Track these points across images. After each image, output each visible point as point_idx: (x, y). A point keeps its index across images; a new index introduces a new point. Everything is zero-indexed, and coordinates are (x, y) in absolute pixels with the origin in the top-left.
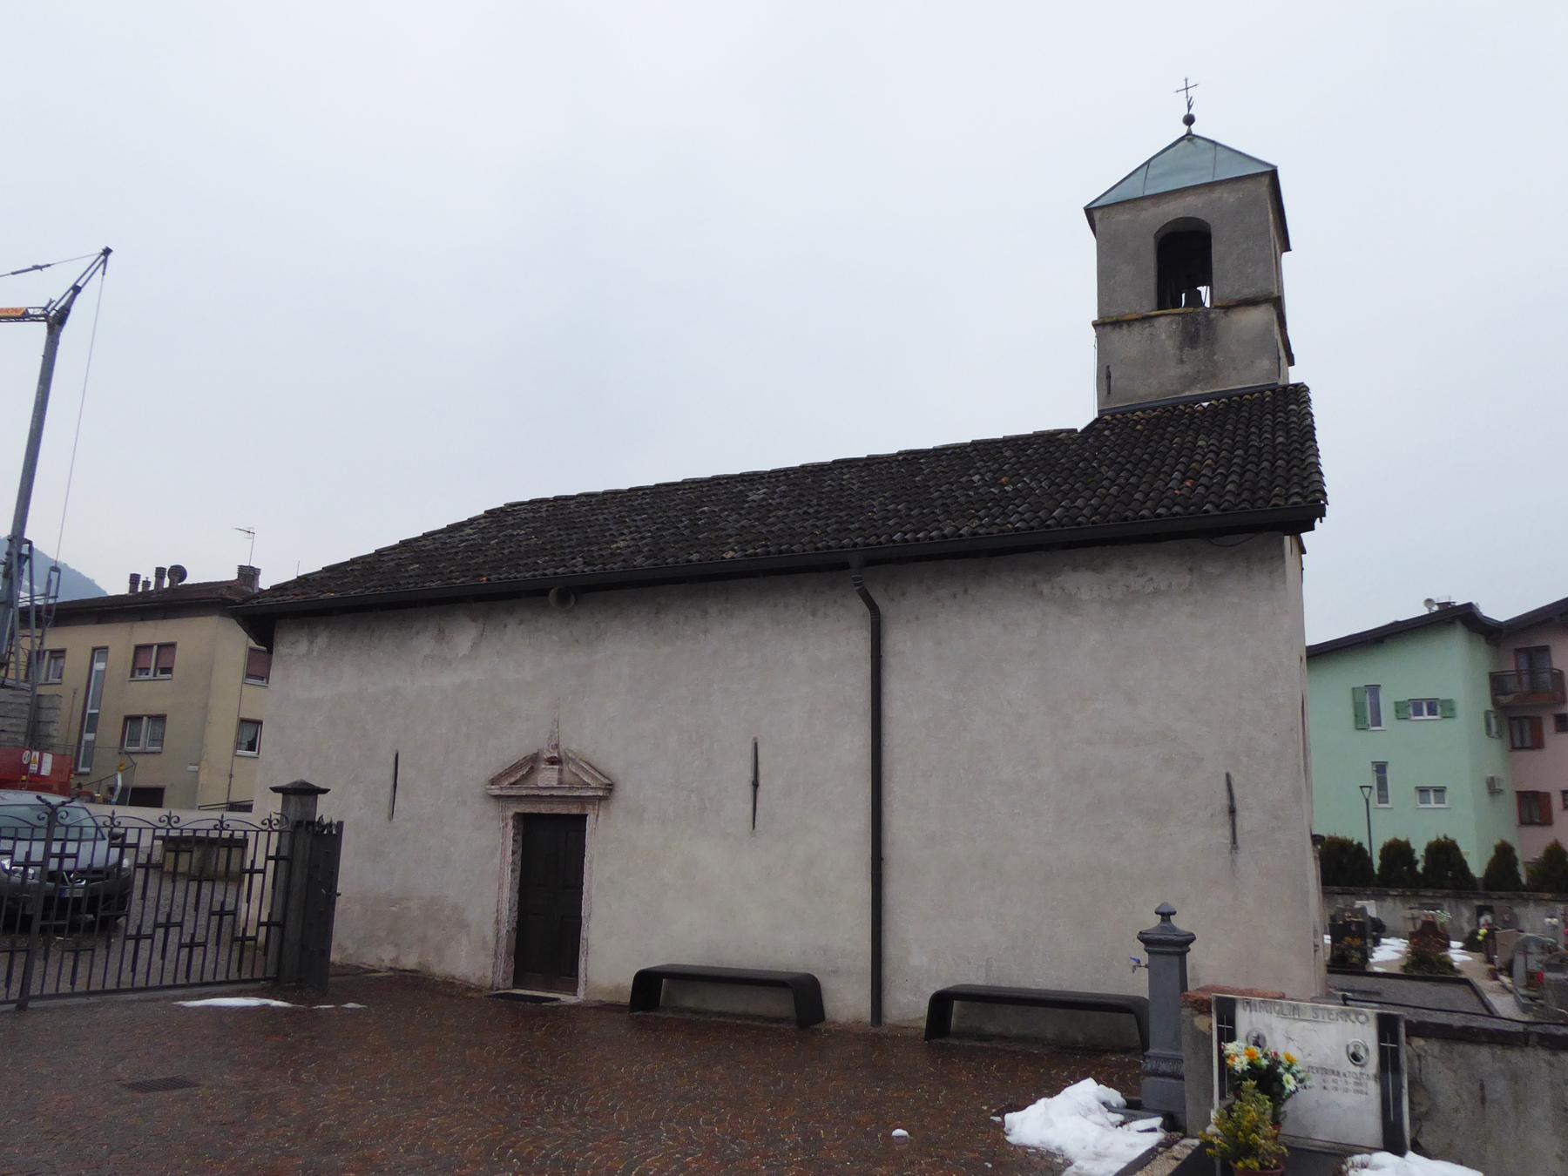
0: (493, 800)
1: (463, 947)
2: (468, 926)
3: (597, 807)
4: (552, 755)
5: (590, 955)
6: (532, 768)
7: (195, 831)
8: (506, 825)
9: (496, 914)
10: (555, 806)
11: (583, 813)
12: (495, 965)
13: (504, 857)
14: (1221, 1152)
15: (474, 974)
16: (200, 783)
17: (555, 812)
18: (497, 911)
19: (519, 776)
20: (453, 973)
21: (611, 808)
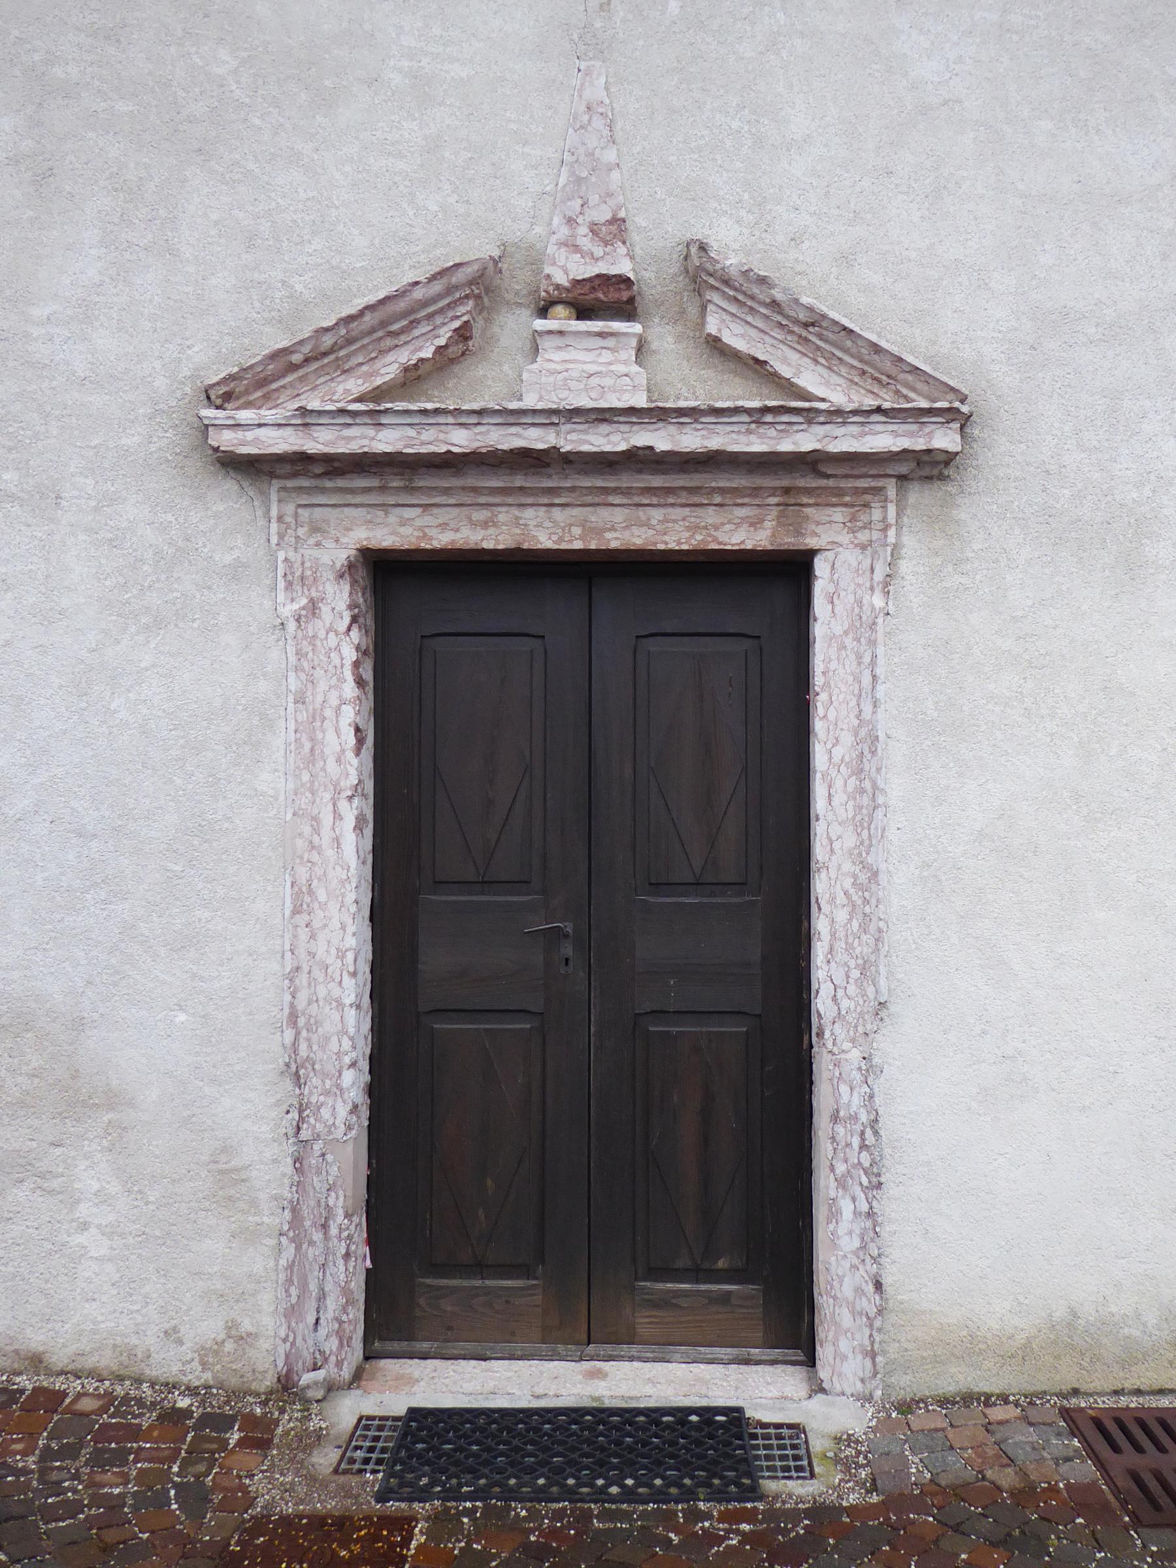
0: (229, 485)
1: (84, 1210)
2: (113, 1100)
3: (892, 510)
4: (602, 268)
5: (891, 1189)
6: (463, 334)
7: (383, 489)
8: (313, 607)
9: (289, 1035)
10: (618, 516)
11: (788, 542)
12: (295, 1273)
13: (313, 756)
14: (1019, 1484)
15: (172, 1334)
16: (669, 10)
17: (614, 541)
18: (293, 1017)
19: (389, 369)
20: (36, 1339)
21: (962, 515)
